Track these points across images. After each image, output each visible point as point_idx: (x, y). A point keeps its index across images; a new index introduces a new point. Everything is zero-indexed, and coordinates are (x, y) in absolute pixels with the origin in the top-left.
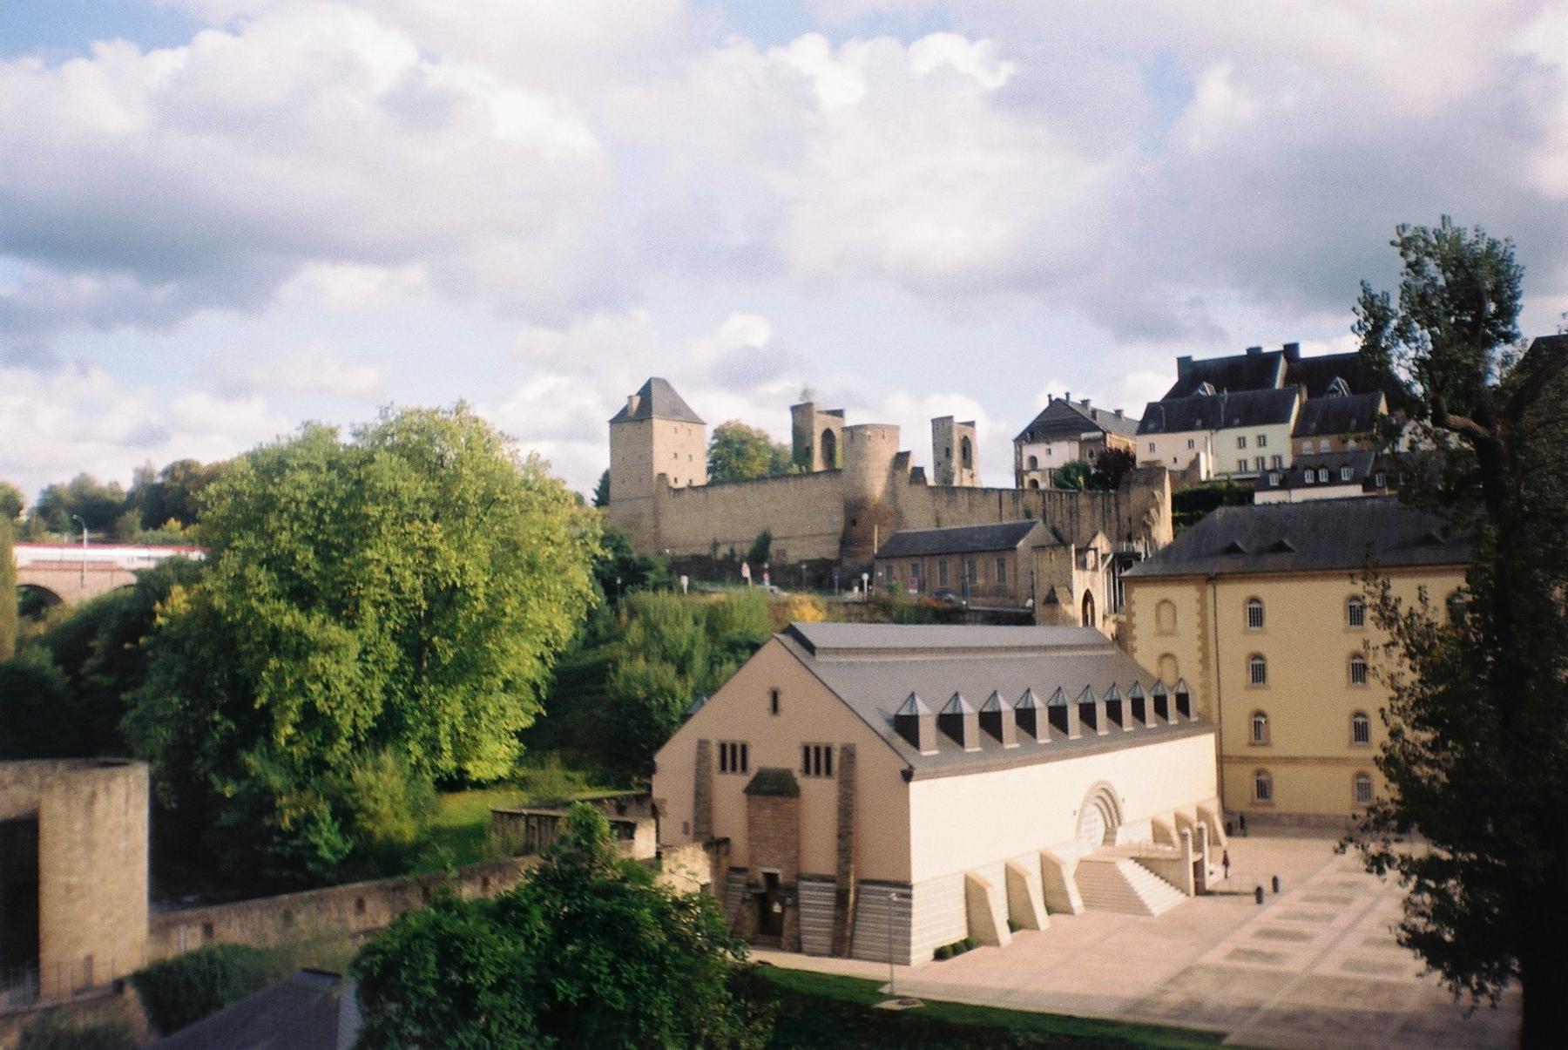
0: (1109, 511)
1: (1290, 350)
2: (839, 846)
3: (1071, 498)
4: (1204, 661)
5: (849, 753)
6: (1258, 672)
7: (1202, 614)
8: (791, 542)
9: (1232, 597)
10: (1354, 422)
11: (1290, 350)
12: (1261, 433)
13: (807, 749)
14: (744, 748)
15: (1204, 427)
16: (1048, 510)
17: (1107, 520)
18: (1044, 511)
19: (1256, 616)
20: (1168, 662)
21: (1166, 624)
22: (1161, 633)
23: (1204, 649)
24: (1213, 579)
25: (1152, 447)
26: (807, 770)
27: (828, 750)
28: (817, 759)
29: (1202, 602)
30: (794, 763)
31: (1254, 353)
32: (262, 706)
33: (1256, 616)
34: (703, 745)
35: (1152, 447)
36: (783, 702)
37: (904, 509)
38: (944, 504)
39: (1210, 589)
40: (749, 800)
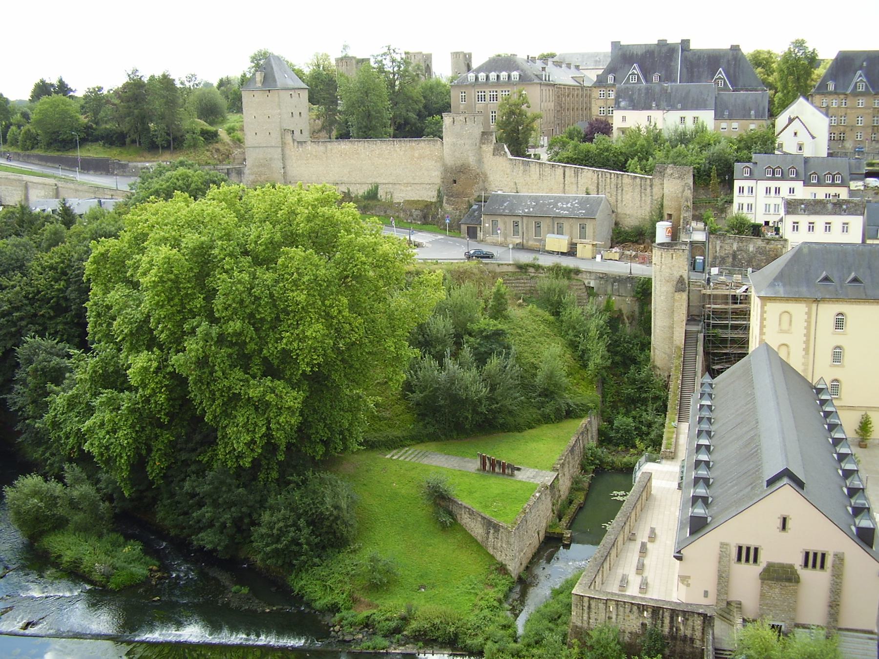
0: (645, 189)
1: (685, 43)
2: (829, 611)
3: (618, 177)
4: (806, 350)
5: (840, 559)
6: (838, 355)
7: (808, 322)
8: (397, 186)
9: (828, 312)
10: (752, 112)
11: (685, 43)
12: (696, 115)
13: (807, 554)
14: (756, 550)
15: (658, 108)
16: (600, 184)
17: (643, 195)
18: (598, 184)
19: (840, 323)
20: (784, 349)
21: (785, 326)
22: (782, 331)
23: (807, 342)
24: (817, 301)
25: (624, 119)
26: (806, 565)
27: (823, 555)
28: (815, 560)
29: (809, 314)
30: (797, 561)
31: (662, 44)
32: (289, 480)
33: (840, 323)
34: (723, 545)
35: (624, 119)
36: (789, 524)
37: (488, 172)
38: (521, 172)
39: (814, 306)
40: (762, 583)
